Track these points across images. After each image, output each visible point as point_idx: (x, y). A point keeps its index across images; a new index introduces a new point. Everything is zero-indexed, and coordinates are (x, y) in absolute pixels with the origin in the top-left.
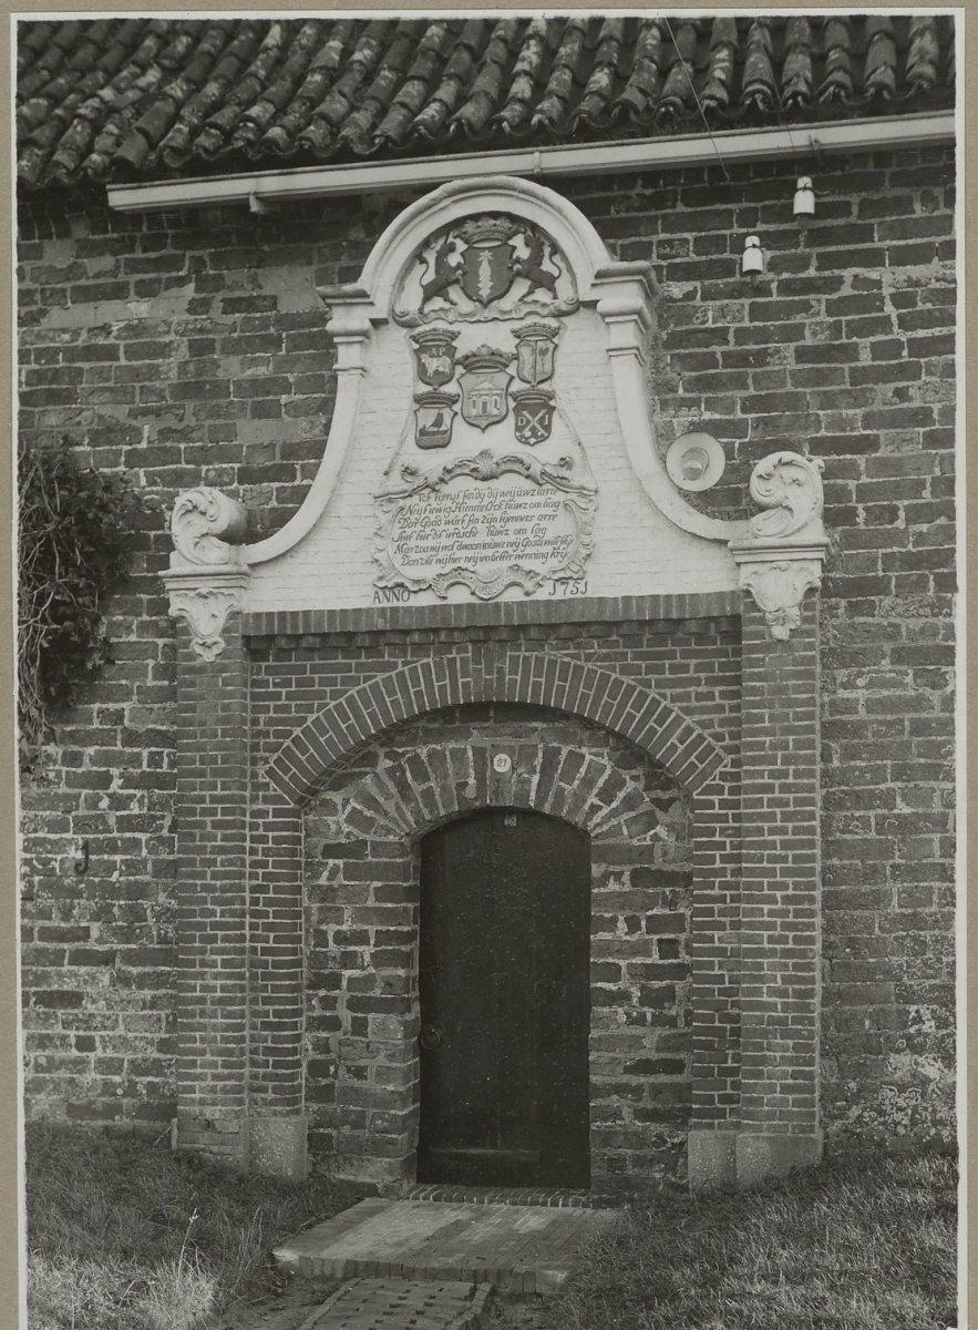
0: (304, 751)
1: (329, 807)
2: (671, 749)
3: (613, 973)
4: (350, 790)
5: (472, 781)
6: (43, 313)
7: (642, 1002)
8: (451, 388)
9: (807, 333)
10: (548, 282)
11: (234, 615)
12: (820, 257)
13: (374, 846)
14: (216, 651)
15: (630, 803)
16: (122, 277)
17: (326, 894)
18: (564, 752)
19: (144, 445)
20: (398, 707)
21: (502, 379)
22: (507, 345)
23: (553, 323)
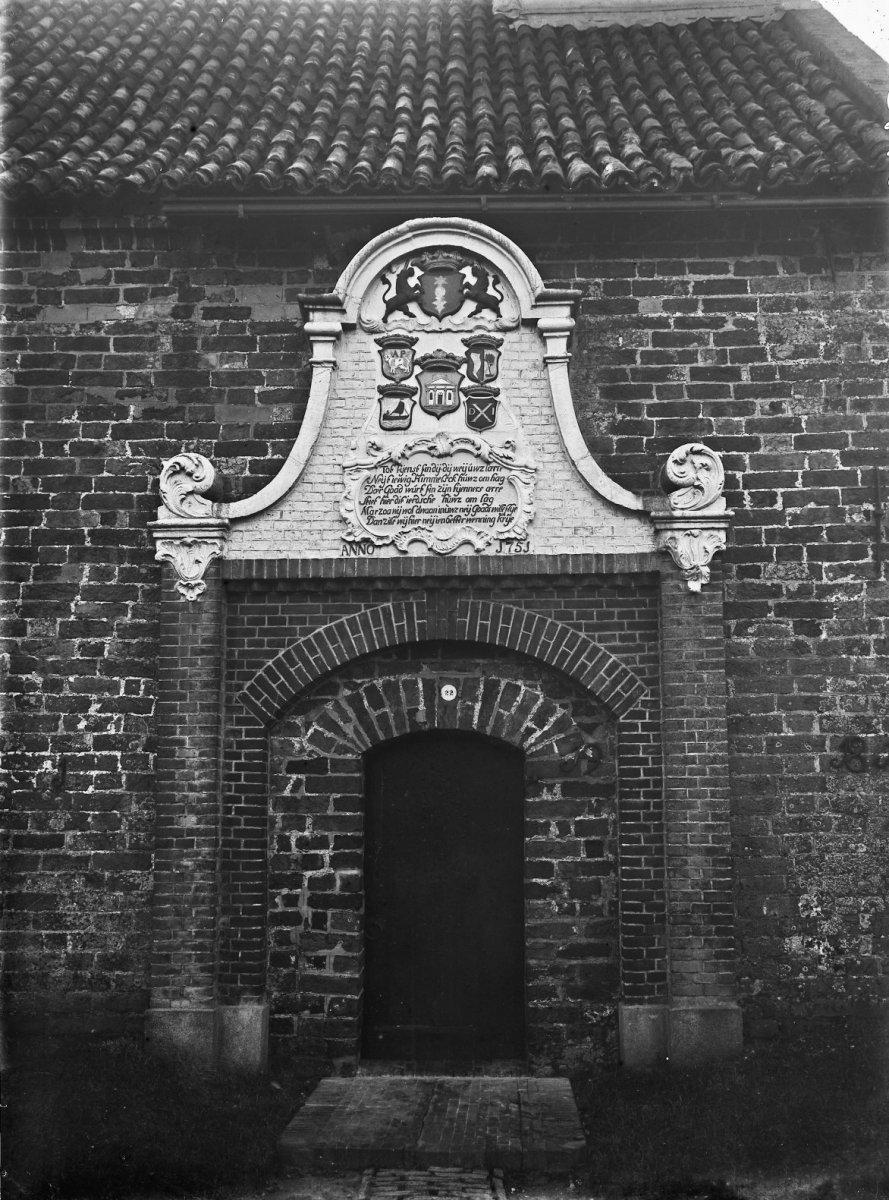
0: (275, 679)
1: (294, 731)
3: (546, 870)
4: (313, 715)
5: (422, 707)
6: (37, 310)
7: (572, 895)
8: (412, 382)
10: (494, 305)
11: (218, 562)
13: (335, 763)
14: (198, 591)
15: (560, 726)
16: (112, 284)
17: (288, 804)
19: (129, 420)
20: (360, 643)
21: (455, 378)
22: (460, 351)
23: (498, 336)
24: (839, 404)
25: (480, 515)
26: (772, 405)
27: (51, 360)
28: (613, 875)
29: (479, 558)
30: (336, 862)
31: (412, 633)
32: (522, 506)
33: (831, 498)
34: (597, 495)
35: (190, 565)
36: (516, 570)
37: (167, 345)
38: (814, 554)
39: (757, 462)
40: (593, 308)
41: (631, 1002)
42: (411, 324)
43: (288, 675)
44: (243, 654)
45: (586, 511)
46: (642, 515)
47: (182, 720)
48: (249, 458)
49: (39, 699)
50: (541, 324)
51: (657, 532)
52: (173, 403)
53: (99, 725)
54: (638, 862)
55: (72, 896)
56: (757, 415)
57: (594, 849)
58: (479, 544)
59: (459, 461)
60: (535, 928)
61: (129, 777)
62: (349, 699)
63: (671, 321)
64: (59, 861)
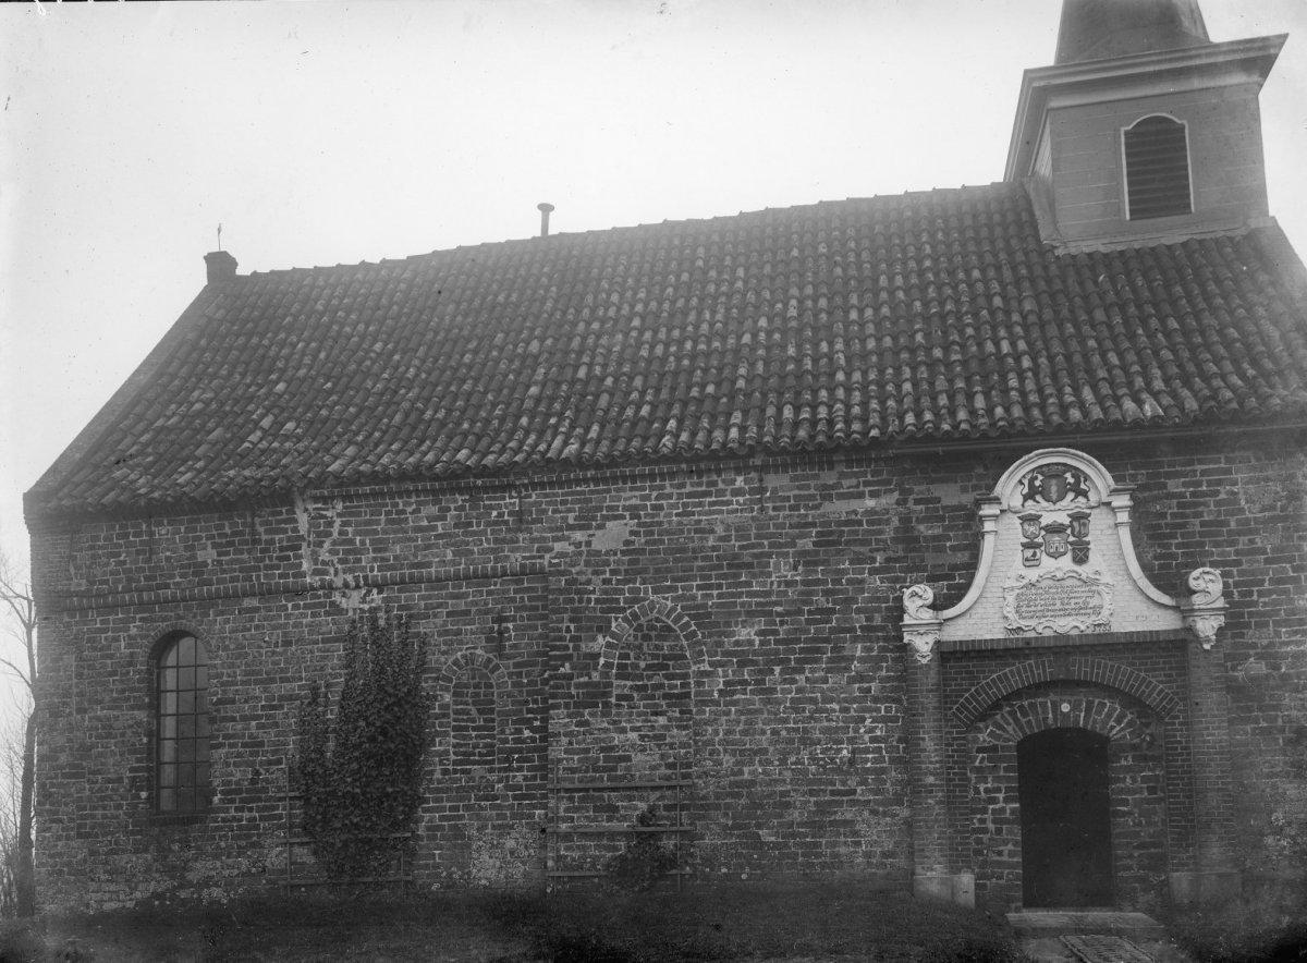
0: (971, 703)
1: (980, 730)
2: (1153, 700)
3: (1125, 802)
4: (989, 722)
5: (1050, 715)
6: (821, 504)
7: (1140, 816)
8: (1040, 540)
9: (1205, 514)
10: (1085, 494)
11: (938, 643)
12: (1207, 481)
13: (1002, 747)
14: (928, 659)
15: (1130, 724)
16: (861, 488)
17: (979, 770)
18: (1097, 701)
19: (877, 564)
20: (1016, 683)
21: (1065, 536)
22: (1067, 521)
23: (1088, 511)
24: (1290, 538)
25: (1082, 611)
26: (1250, 540)
27: (831, 533)
28: (1163, 804)
29: (1082, 636)
30: (1006, 800)
31: (1045, 677)
32: (1106, 606)
33: (1286, 592)
34: (1148, 598)
35: (923, 645)
36: (1103, 641)
37: (895, 522)
38: (1277, 624)
39: (1241, 573)
40: (1143, 488)
41: (1177, 871)
42: (1038, 507)
43: (977, 701)
44: (952, 691)
45: (1141, 606)
46: (1176, 608)
47: (923, 727)
48: (945, 583)
49: (838, 717)
50: (1114, 504)
51: (1184, 617)
52: (901, 554)
53: (872, 730)
54: (1178, 797)
55: (863, 821)
56: (1240, 547)
57: (1152, 790)
58: (1083, 627)
59: (1069, 582)
60: (1120, 833)
61: (890, 758)
62: (1009, 712)
63: (1188, 494)
64: (854, 803)
